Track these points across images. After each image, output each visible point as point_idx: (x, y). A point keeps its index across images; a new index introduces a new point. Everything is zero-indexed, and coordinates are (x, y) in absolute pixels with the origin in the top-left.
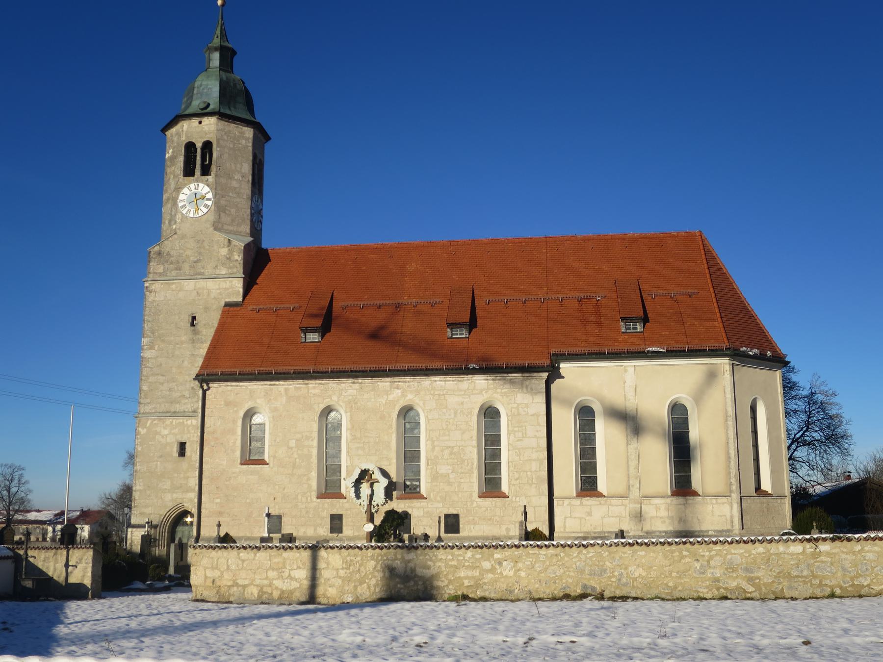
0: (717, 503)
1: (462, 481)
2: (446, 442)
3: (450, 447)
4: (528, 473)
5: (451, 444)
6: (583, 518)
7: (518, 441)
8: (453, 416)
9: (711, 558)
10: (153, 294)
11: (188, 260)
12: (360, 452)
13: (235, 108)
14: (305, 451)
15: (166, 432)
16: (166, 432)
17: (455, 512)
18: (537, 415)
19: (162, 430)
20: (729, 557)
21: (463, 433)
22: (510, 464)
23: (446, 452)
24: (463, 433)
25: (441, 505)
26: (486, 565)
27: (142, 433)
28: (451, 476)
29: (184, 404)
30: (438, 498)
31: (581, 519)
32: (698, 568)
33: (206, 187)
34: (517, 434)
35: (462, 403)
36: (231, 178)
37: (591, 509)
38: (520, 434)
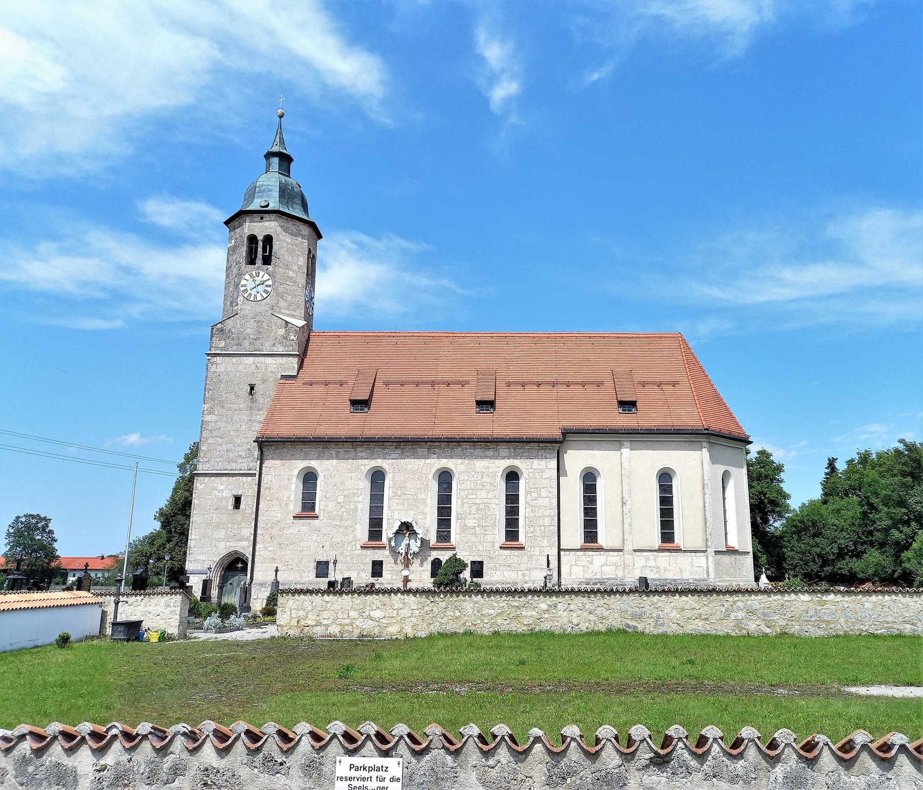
0: (695, 556)
1: (486, 533)
2: (474, 500)
3: (477, 504)
4: (542, 527)
5: (478, 501)
6: (586, 566)
7: (534, 500)
8: (480, 478)
9: (734, 602)
10: (215, 366)
11: (248, 338)
12: (400, 507)
13: (293, 208)
14: (352, 506)
15: (222, 487)
16: (222, 487)
17: (480, 560)
18: (550, 478)
19: (219, 485)
20: (749, 603)
21: (488, 493)
22: (527, 519)
23: (474, 507)
24: (488, 493)
25: (468, 553)
26: (544, 606)
27: (200, 488)
28: (477, 529)
29: (241, 463)
30: (466, 547)
31: (583, 566)
32: (724, 611)
33: (266, 274)
34: (532, 494)
35: (488, 467)
36: (287, 269)
37: (592, 558)
38: (536, 494)
